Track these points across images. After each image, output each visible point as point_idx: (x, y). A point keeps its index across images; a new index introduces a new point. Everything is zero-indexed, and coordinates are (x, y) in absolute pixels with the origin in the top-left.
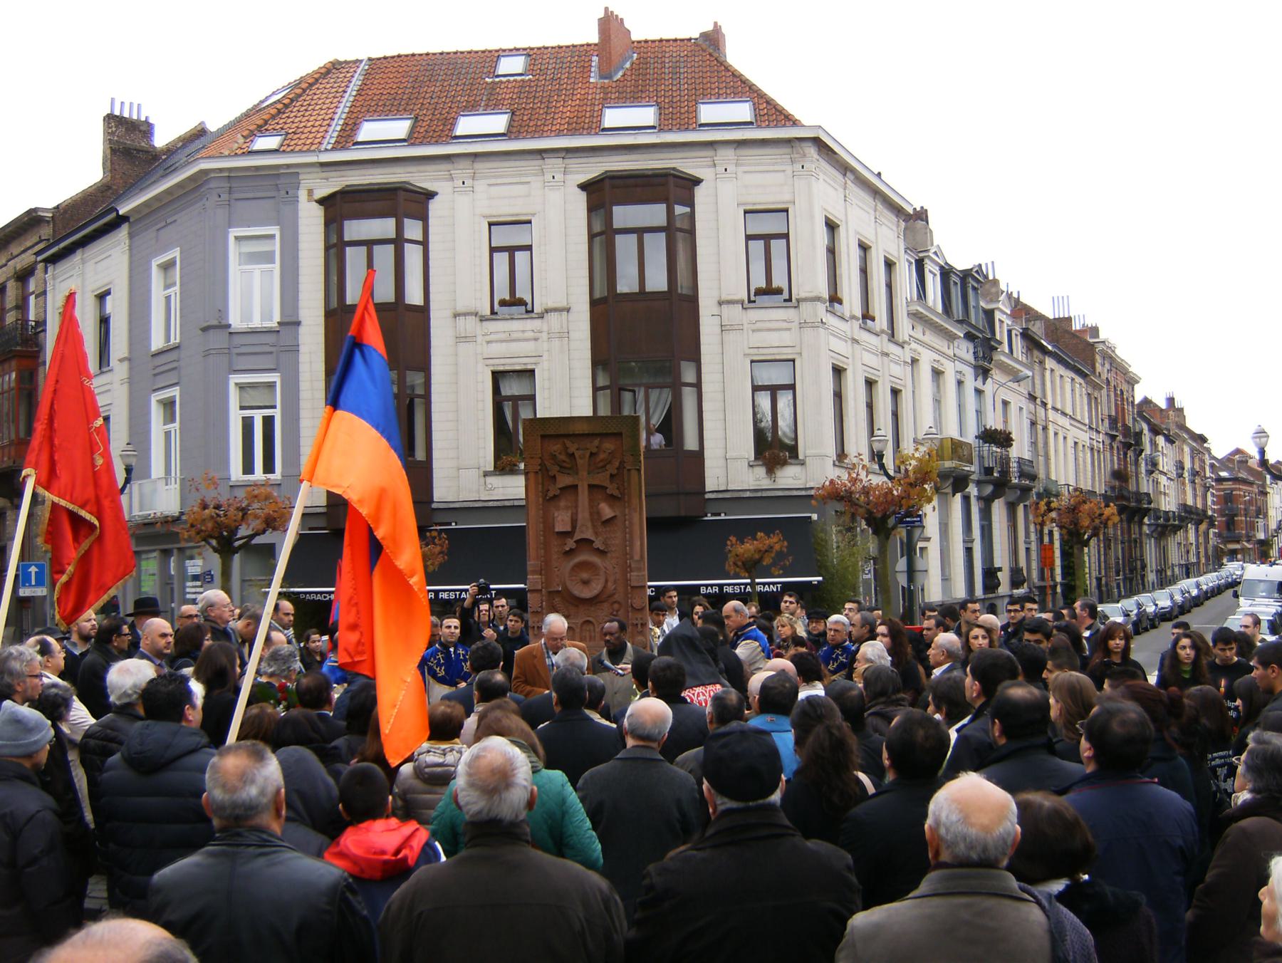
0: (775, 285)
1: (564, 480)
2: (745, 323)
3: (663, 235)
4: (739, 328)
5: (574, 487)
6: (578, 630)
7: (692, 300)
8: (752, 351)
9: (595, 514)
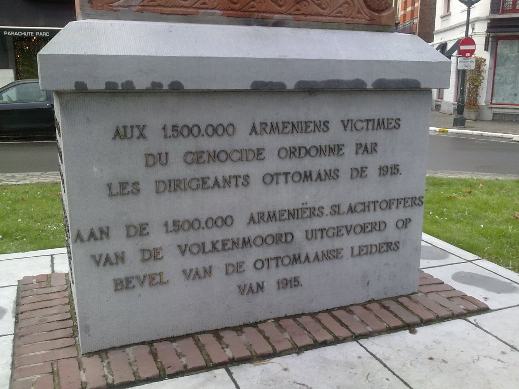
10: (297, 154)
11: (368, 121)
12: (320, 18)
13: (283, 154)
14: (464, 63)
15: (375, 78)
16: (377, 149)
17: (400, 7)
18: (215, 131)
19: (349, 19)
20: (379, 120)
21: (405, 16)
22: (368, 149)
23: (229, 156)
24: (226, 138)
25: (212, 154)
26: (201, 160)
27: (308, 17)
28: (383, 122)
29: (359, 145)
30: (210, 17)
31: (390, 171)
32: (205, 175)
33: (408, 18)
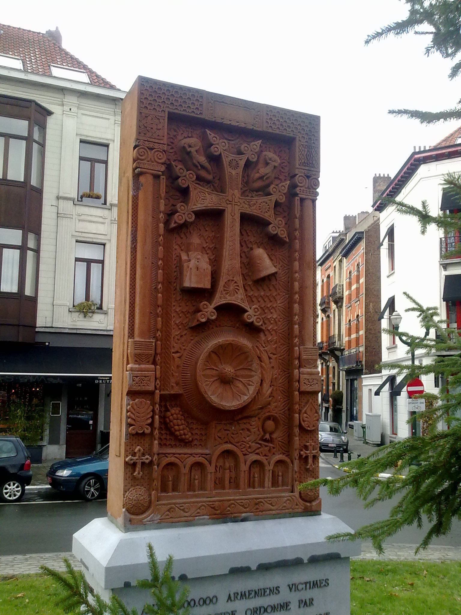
0: (96, 192)
1: (203, 199)
2: (74, 214)
3: (24, 142)
5: (214, 216)
6: (211, 469)
7: (39, 192)
8: (77, 234)
9: (249, 264)
10: (258, 612)
11: (306, 583)
12: (271, 512)
14: (414, 405)
15: (309, 555)
17: (344, 333)
18: (205, 602)
20: (313, 582)
21: (349, 342)
24: (211, 605)
27: (264, 512)
28: (317, 583)
29: (300, 601)
33: (353, 344)
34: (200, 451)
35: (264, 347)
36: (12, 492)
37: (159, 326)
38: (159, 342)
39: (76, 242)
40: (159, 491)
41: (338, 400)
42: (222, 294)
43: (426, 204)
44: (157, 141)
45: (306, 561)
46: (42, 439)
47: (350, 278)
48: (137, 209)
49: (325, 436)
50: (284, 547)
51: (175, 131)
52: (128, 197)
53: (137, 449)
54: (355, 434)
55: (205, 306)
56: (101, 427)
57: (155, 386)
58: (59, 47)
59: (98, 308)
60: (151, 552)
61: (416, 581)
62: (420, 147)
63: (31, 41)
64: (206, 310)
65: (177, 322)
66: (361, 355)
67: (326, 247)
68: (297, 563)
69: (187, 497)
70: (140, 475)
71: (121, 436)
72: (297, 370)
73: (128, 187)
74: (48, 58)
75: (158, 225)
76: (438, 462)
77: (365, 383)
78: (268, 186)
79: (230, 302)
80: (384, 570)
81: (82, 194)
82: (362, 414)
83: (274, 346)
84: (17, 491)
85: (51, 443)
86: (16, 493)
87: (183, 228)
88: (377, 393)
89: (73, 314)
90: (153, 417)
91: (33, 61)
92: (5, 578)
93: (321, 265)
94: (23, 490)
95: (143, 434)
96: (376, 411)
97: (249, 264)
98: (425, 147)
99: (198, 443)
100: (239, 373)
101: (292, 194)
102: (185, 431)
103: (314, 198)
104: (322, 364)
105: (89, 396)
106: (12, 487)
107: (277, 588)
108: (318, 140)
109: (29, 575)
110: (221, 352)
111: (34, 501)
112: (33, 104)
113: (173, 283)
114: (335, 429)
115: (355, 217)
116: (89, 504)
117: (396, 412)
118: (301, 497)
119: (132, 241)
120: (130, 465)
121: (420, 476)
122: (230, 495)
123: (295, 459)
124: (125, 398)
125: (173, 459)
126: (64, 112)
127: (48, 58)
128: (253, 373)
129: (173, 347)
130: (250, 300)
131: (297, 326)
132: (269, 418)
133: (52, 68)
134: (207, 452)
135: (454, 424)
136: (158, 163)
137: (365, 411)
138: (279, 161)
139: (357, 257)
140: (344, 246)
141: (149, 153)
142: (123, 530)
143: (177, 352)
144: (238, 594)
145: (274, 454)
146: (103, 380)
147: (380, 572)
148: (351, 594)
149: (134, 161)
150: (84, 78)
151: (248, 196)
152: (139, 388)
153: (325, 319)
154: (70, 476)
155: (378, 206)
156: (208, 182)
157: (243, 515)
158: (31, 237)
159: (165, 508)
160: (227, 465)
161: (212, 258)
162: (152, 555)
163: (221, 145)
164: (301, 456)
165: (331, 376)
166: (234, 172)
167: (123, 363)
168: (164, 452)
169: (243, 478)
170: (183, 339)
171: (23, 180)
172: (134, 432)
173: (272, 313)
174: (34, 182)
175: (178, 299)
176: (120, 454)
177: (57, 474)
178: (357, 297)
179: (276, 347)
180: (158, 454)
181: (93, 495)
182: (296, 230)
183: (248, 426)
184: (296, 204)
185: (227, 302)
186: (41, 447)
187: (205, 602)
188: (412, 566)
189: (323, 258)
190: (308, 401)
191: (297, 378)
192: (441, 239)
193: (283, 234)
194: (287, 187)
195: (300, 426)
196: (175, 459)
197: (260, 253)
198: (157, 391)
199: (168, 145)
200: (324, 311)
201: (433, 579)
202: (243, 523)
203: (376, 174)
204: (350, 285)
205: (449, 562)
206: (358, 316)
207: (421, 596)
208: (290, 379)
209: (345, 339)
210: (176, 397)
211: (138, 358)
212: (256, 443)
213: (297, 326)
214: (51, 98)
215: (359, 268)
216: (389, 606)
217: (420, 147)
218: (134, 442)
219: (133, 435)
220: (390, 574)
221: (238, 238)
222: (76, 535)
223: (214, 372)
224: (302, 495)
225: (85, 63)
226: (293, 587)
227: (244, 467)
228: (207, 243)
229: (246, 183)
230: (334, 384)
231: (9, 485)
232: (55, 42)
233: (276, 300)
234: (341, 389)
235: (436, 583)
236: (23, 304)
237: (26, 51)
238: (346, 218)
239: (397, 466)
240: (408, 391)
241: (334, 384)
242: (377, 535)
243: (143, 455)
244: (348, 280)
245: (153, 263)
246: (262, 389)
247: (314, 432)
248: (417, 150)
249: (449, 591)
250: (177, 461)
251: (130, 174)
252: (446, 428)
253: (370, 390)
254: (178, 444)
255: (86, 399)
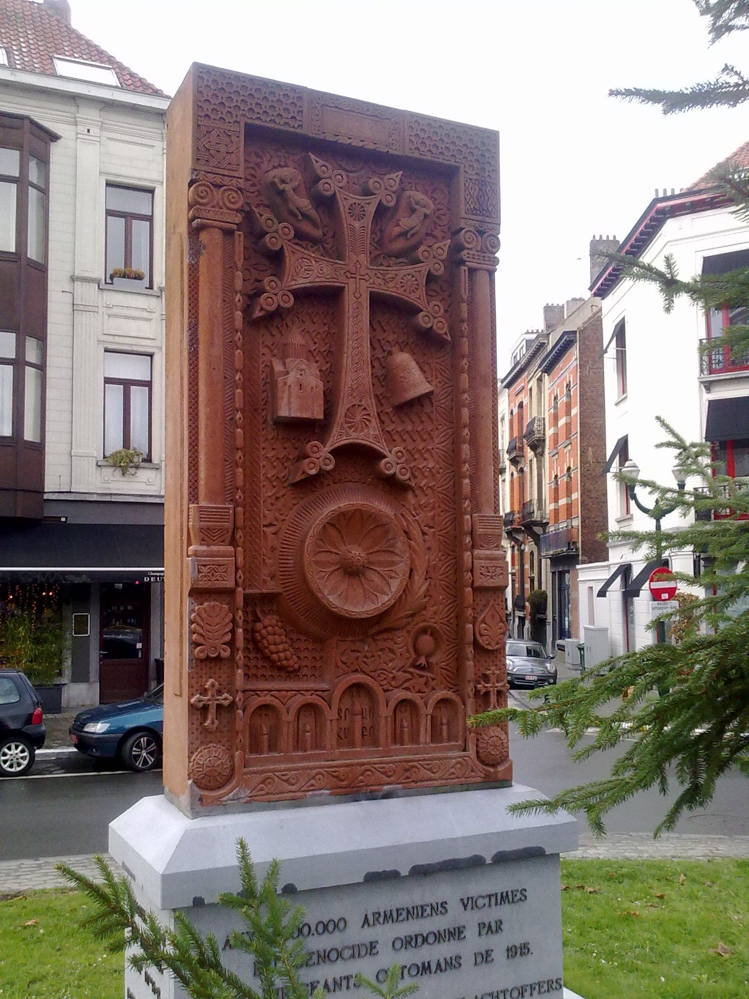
1: (307, 270)
2: (100, 305)
3: (14, 187)
4: (91, 310)
5: (326, 298)
6: (331, 714)
7: (41, 269)
8: (106, 338)
9: (386, 379)
10: (413, 943)
11: (490, 896)
13: (398, 944)
15: (494, 852)
16: (503, 927)
17: (548, 497)
18: (326, 928)
19: (463, 779)
20: (502, 893)
21: (556, 512)
22: (491, 928)
23: (340, 955)
24: (337, 934)
25: (322, 954)
26: (311, 963)
27: (419, 784)
29: (481, 925)
30: (317, 798)
31: (519, 951)
32: (315, 979)
33: (563, 515)
34: (312, 685)
35: (414, 516)
36: (15, 760)
37: (240, 482)
38: (240, 509)
39: (105, 351)
40: (247, 750)
41: (539, 606)
42: (342, 427)
43: (672, 261)
44: (226, 173)
45: (489, 861)
46: (60, 674)
47: (555, 408)
48: (197, 288)
49: (517, 662)
50: (453, 839)
51: (258, 156)
52: (182, 269)
53: (209, 683)
54: (568, 659)
55: (315, 449)
56: (155, 655)
57: (236, 581)
58: (66, 26)
59: (144, 461)
60: (243, 852)
61: (668, 892)
62: (665, 191)
63: (19, 16)
64: (317, 455)
65: (270, 476)
66: (574, 531)
67: (515, 357)
68: (475, 863)
69: (292, 760)
70: (215, 726)
71: (181, 663)
72: (469, 553)
73: (182, 251)
74: (49, 45)
75: (232, 313)
76: (697, 688)
77: (582, 576)
78: (416, 247)
79: (357, 441)
80: (616, 875)
81: (112, 272)
82: (578, 628)
83: (432, 514)
84: (22, 758)
85: (75, 679)
86: (21, 761)
87: (275, 317)
88: (602, 593)
89: (104, 470)
90: (233, 632)
91: (24, 50)
92: (6, 897)
93: (508, 386)
94: (32, 756)
95: (218, 659)
96: (601, 622)
97: (386, 379)
98: (673, 190)
99: (309, 673)
100: (374, 558)
101: (454, 261)
102: (288, 654)
103: (490, 267)
104: (513, 547)
105: (134, 603)
106: (13, 751)
107: (444, 904)
108: (496, 171)
109: (44, 892)
110: (343, 523)
111: (51, 773)
112: (26, 122)
113: (259, 411)
114: (535, 651)
115: (563, 307)
116: (140, 775)
117: (633, 622)
118: (478, 757)
119: (191, 340)
120: (198, 709)
121: (666, 711)
122: (366, 757)
123: (469, 697)
124: (187, 600)
125: (268, 699)
126: (79, 136)
127: (49, 45)
128: (396, 559)
129: (265, 516)
130: (390, 437)
131: (467, 481)
132: (424, 631)
133: (56, 62)
134: (325, 686)
135: (722, 626)
136: (229, 209)
137: (583, 622)
138: (433, 207)
139: (567, 373)
140: (545, 355)
141: (215, 193)
142: (189, 815)
143: (271, 525)
144: (379, 914)
145: (433, 689)
146: (156, 576)
147: (610, 878)
148: (564, 914)
149: (190, 207)
150: (109, 77)
151: (381, 265)
152: (208, 585)
153: (516, 475)
154: (108, 732)
155: (598, 289)
156: (315, 241)
157: (386, 787)
158: (31, 345)
159: (258, 778)
160: (358, 708)
161: (324, 369)
162: (244, 857)
163: (334, 179)
164: (477, 692)
165: (527, 566)
166: (357, 225)
167: (182, 543)
168: (254, 688)
169: (385, 729)
170: (279, 504)
171: (14, 251)
172: (203, 656)
173: (425, 460)
174: (32, 253)
175: (270, 437)
176: (181, 691)
177: (86, 730)
178: (568, 438)
179: (434, 516)
180: (243, 692)
181: (145, 762)
182: (463, 321)
183: (390, 644)
184: (463, 278)
185: (351, 441)
186: (60, 687)
187: (326, 928)
188: (661, 868)
189: (512, 375)
190: (488, 602)
191: (470, 565)
192: (701, 340)
193: (441, 328)
194: (446, 249)
195: (476, 643)
196: (273, 698)
197: (404, 359)
198: (240, 589)
199: (247, 180)
200: (514, 461)
201: (696, 887)
202: (385, 801)
203: (594, 237)
204: (556, 418)
205: (719, 860)
206: (569, 469)
207: (675, 915)
208: (457, 567)
209: (550, 507)
210: (270, 599)
211: (207, 535)
212: (405, 672)
213: (467, 481)
214: (56, 113)
215: (569, 390)
216: (625, 932)
217: (665, 191)
218: (204, 672)
219: (201, 661)
220: (626, 880)
221: (366, 335)
222: (113, 825)
223: (333, 556)
224: (481, 755)
225: (111, 53)
226: (467, 903)
227: (386, 712)
228: (315, 343)
229: (379, 243)
230: (532, 580)
231: (9, 749)
232: (59, 18)
233: (432, 438)
234: (543, 588)
235: (700, 894)
236: (23, 455)
237: (12, 33)
238: (548, 309)
239: (626, 695)
240: (651, 590)
241: (532, 580)
242: (594, 804)
243: (219, 692)
244: (552, 410)
245: (225, 378)
246: (412, 584)
247: (497, 654)
248: (661, 195)
249: (720, 906)
250: (276, 702)
251: (183, 228)
252: (713, 633)
253: (591, 588)
254: (275, 673)
255: (130, 608)
